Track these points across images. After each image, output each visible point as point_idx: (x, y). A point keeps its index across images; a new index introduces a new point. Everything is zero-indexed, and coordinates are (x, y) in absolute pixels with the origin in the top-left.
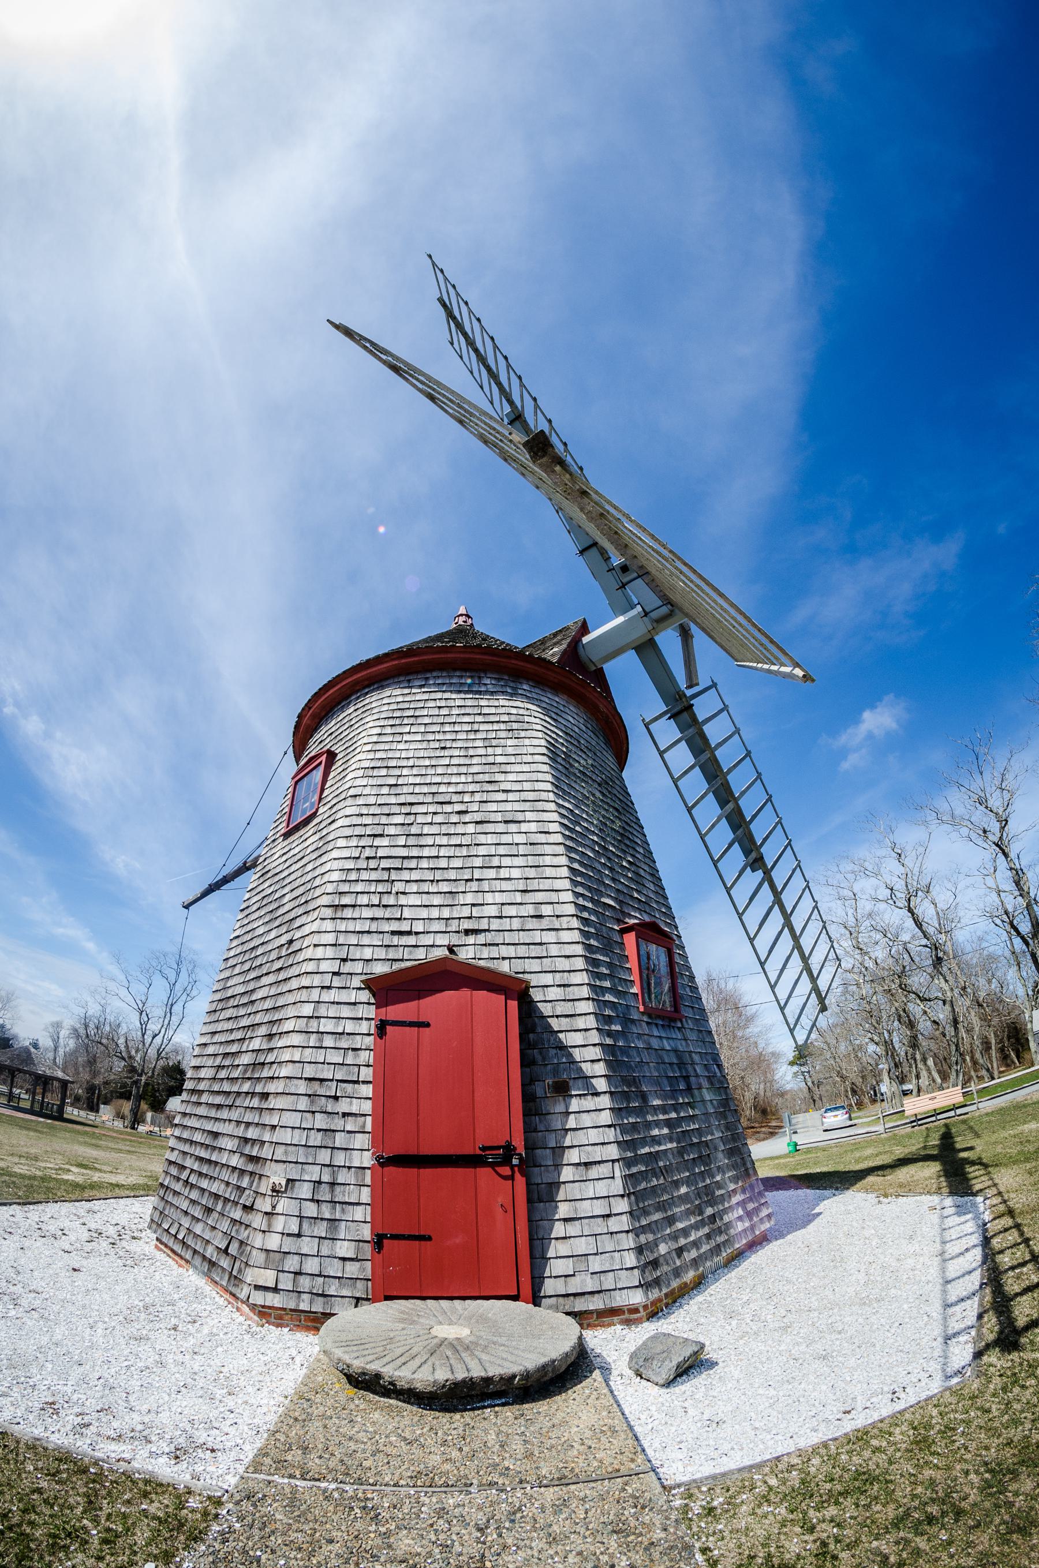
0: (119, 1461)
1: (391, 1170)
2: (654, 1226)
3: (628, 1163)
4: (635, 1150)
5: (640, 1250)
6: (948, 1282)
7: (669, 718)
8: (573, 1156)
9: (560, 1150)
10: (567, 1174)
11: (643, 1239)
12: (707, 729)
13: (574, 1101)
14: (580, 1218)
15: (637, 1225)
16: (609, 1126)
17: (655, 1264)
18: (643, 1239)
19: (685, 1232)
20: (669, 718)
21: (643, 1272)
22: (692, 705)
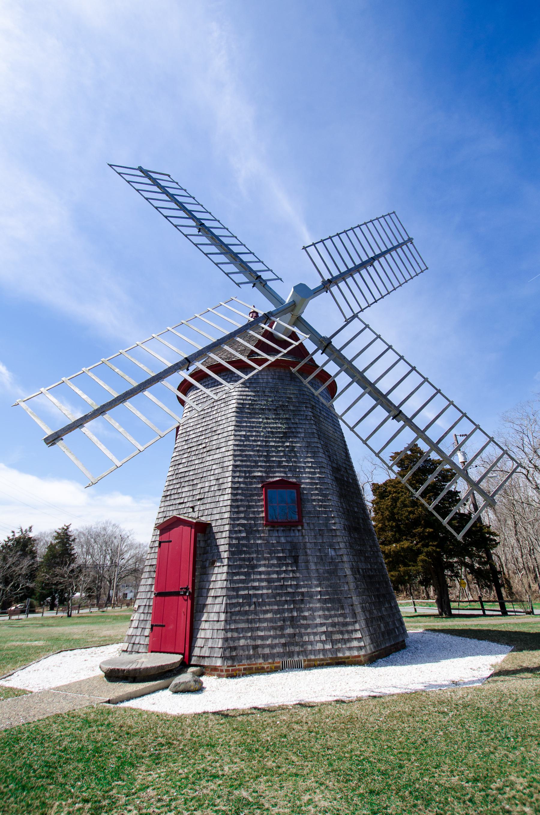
0: (54, 666)
1: (158, 598)
2: (240, 630)
3: (229, 597)
4: (237, 592)
5: (226, 640)
6: (201, 647)
7: (393, 419)
8: (212, 593)
9: (209, 590)
10: (209, 601)
11: (229, 635)
12: (378, 386)
13: (216, 569)
14: (210, 621)
15: (228, 627)
16: (225, 580)
17: (235, 648)
18: (229, 635)
19: (262, 638)
20: (393, 419)
21: (225, 650)
22: (331, 342)
